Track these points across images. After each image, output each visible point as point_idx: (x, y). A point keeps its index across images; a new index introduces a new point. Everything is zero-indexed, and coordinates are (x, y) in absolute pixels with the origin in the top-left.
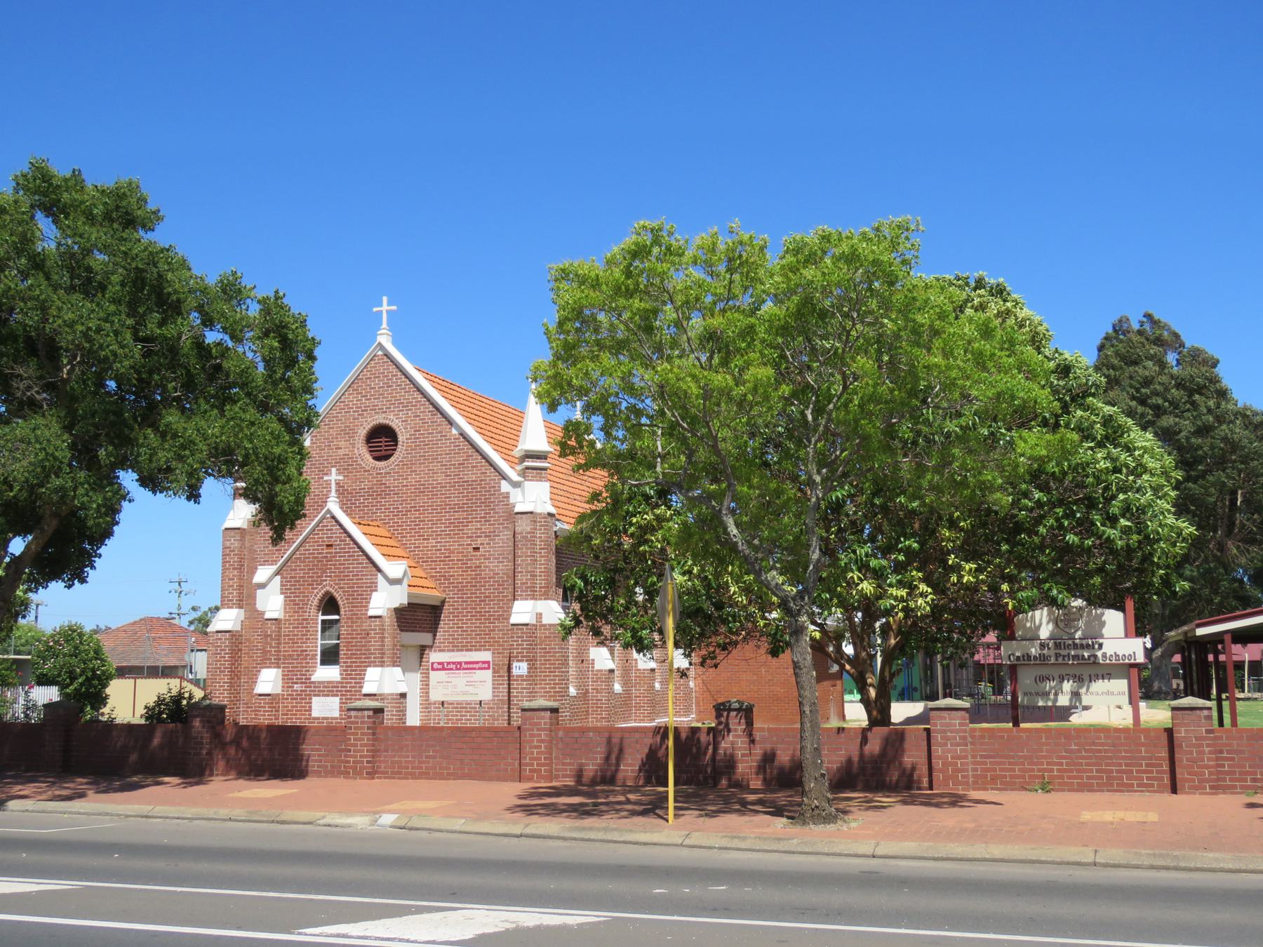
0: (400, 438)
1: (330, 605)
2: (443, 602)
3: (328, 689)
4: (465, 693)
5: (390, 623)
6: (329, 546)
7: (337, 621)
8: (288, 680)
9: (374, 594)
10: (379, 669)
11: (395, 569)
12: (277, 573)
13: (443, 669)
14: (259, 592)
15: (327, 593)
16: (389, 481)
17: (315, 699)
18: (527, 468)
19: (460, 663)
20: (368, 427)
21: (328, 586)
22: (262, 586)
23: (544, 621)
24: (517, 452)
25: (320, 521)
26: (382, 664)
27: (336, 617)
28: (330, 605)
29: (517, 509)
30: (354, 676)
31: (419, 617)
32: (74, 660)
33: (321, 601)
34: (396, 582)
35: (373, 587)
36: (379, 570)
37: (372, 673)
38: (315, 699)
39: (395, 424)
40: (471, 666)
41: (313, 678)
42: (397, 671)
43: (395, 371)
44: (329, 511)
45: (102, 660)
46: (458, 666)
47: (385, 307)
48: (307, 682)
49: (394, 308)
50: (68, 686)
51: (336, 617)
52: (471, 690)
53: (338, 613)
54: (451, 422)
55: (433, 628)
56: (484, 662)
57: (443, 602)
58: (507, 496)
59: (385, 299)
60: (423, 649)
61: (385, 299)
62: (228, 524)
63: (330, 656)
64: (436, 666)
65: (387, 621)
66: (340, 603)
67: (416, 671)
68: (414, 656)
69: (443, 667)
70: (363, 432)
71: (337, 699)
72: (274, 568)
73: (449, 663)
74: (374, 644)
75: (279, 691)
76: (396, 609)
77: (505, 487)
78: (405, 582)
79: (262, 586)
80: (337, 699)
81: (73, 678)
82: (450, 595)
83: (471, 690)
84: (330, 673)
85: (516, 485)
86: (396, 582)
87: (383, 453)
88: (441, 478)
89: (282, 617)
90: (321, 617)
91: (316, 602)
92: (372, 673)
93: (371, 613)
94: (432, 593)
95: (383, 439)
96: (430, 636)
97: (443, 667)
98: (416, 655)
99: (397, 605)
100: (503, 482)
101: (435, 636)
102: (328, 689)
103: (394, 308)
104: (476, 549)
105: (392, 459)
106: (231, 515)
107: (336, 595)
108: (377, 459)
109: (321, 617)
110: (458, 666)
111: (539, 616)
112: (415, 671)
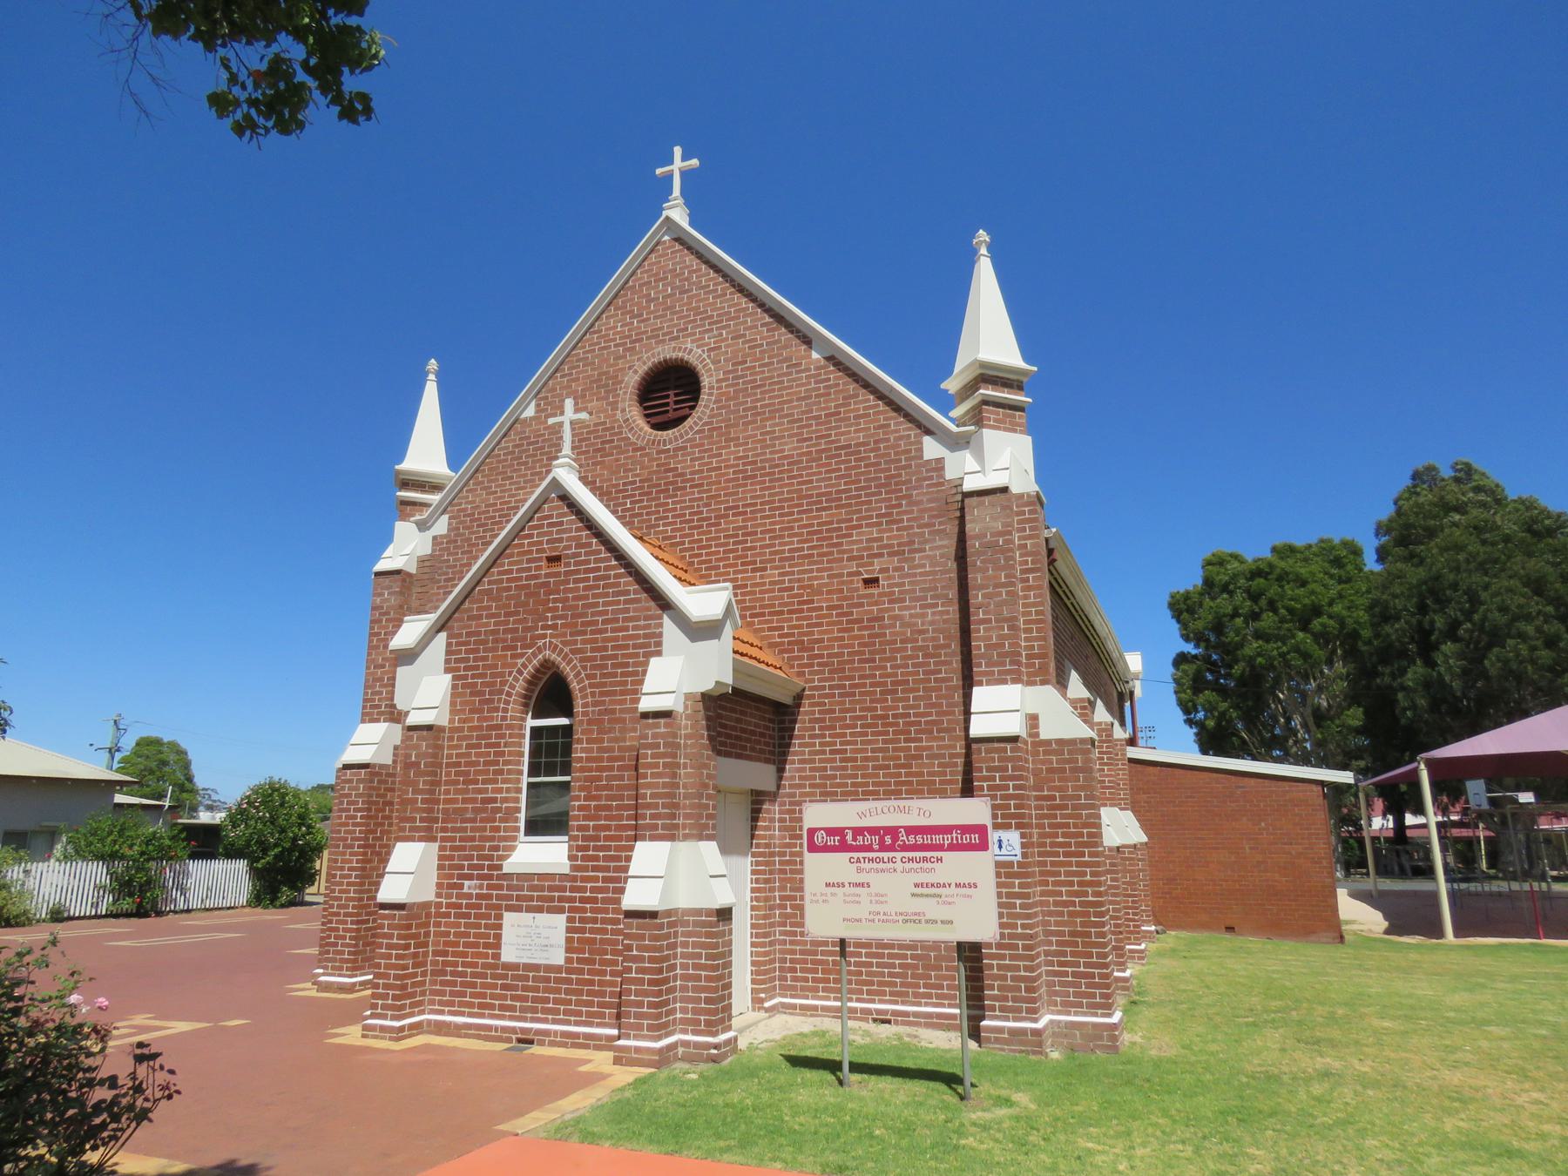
0: (706, 381)
1: (551, 693)
2: (799, 697)
3: (539, 893)
5: (691, 731)
6: (551, 560)
7: (568, 730)
8: (450, 872)
9: (654, 661)
10: (665, 846)
11: (705, 601)
12: (440, 627)
13: (843, 847)
14: (402, 672)
15: (546, 665)
16: (683, 464)
17: (508, 918)
18: (985, 402)
19: (893, 831)
21: (550, 648)
22: (408, 656)
23: (1046, 733)
24: (952, 385)
26: (670, 834)
27: (564, 721)
28: (551, 693)
31: (748, 722)
33: (531, 683)
36: (664, 603)
37: (648, 856)
38: (508, 918)
39: (693, 352)
45: (309, 827)
46: (888, 839)
47: (678, 164)
48: (491, 872)
49: (695, 162)
50: (257, 860)
51: (564, 721)
52: (930, 908)
53: (568, 712)
54: (807, 340)
55: (778, 755)
56: (966, 829)
57: (799, 697)
58: (939, 465)
59: (678, 151)
60: (757, 801)
61: (678, 151)
64: (820, 838)
65: (685, 726)
68: (738, 813)
69: (840, 841)
71: (560, 921)
72: (432, 617)
73: (858, 831)
74: (652, 783)
75: (428, 894)
76: (706, 697)
78: (728, 631)
80: (560, 921)
81: (265, 851)
82: (813, 681)
83: (930, 908)
84: (543, 855)
85: (957, 443)
87: (672, 415)
88: (789, 447)
89: (444, 721)
90: (531, 723)
91: (520, 686)
92: (648, 856)
93: (646, 704)
94: (777, 677)
95: (671, 393)
97: (840, 841)
98: (742, 812)
99: (707, 685)
100: (927, 440)
101: (781, 770)
102: (539, 893)
104: (871, 582)
105: (689, 421)
106: (388, 552)
107: (566, 669)
109: (531, 723)
110: (888, 839)
111: (1033, 720)
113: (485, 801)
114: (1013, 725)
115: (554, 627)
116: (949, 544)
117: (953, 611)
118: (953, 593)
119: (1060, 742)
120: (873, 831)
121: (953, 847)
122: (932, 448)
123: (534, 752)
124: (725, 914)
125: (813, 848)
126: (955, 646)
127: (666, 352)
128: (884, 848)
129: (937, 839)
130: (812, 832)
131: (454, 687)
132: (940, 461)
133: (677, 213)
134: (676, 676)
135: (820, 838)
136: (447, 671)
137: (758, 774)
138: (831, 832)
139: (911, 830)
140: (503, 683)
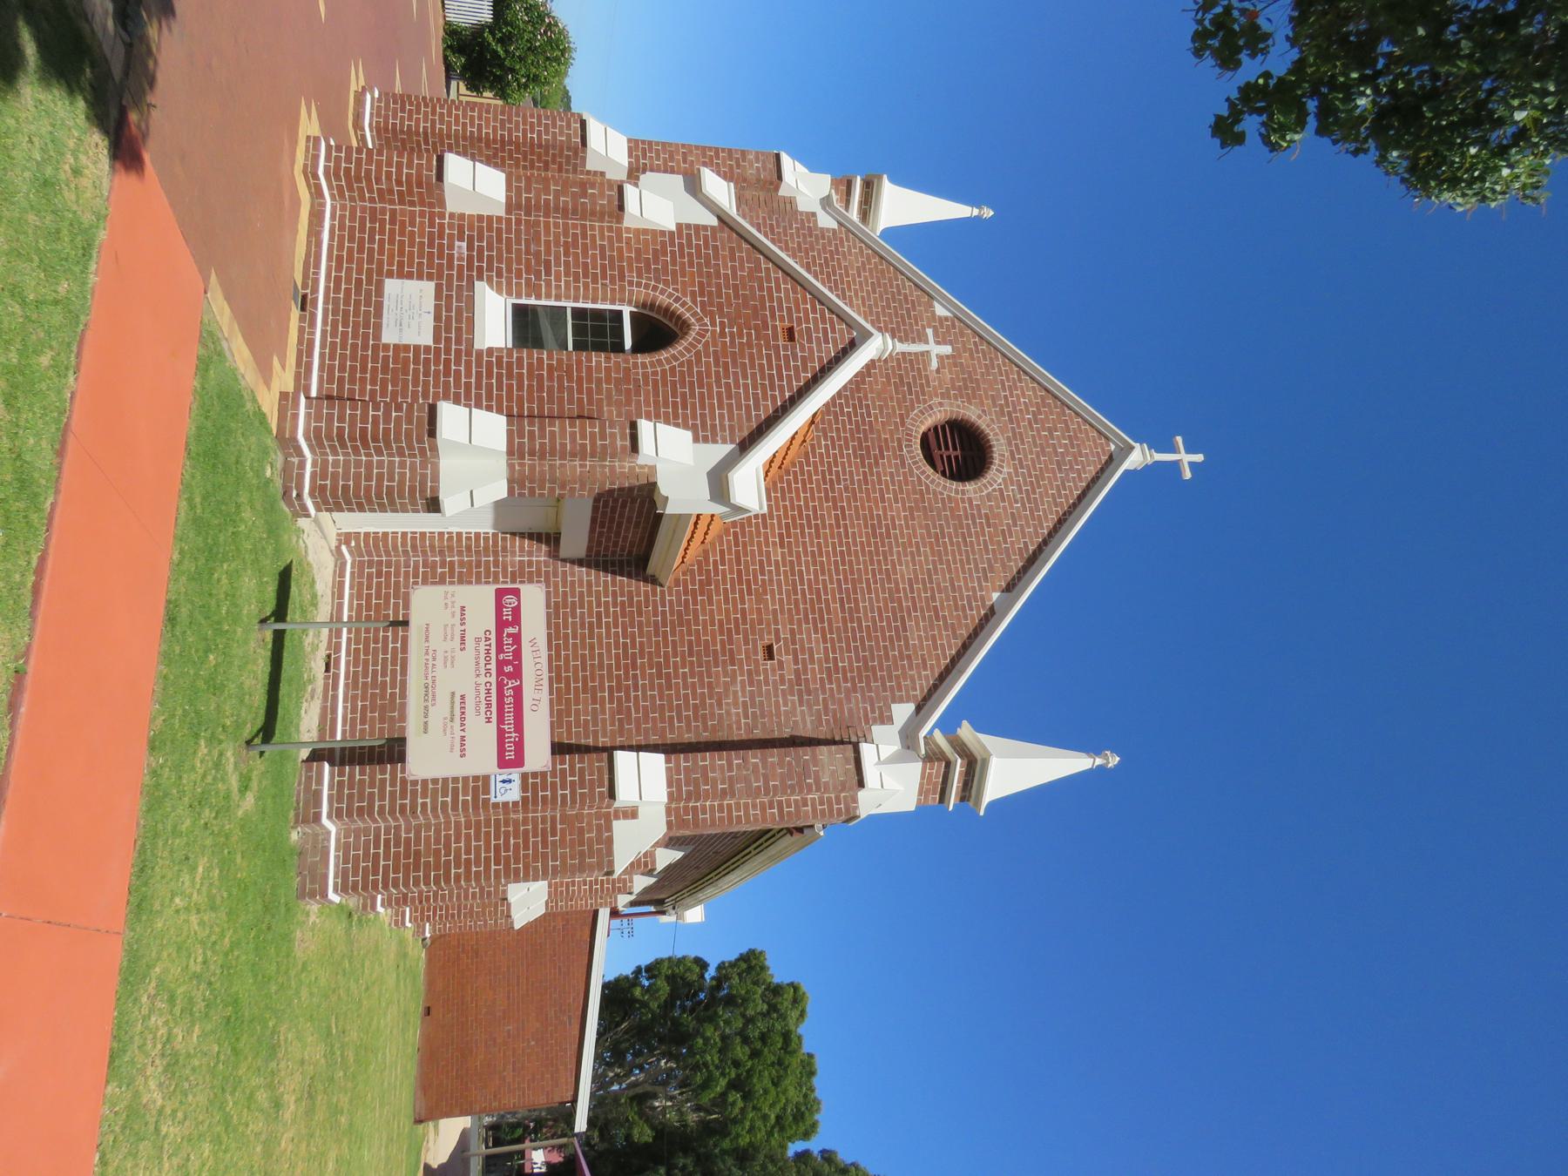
0: (970, 487)
1: (656, 332)
2: (654, 581)
3: (454, 317)
4: (429, 691)
5: (618, 472)
7: (618, 347)
8: (477, 228)
9: (689, 434)
10: (502, 446)
12: (724, 220)
13: (501, 624)
14: (678, 180)
15: (685, 326)
16: (887, 466)
17: (429, 287)
18: (948, 764)
19: (517, 674)
20: (982, 424)
21: (701, 330)
23: (618, 825)
24: (966, 731)
25: (842, 317)
27: (628, 344)
28: (656, 332)
29: (865, 748)
30: (483, 383)
31: (628, 530)
32: (523, 44)
33: (666, 311)
34: (718, 483)
35: (702, 435)
36: (746, 445)
37: (492, 428)
38: (429, 287)
39: (998, 474)
40: (508, 708)
41: (481, 287)
42: (499, 490)
43: (1088, 476)
44: (867, 336)
46: (509, 668)
48: (476, 269)
49: (1188, 475)
50: (492, 33)
51: (628, 344)
52: (440, 711)
53: (637, 348)
54: (1011, 587)
55: (599, 559)
56: (519, 746)
57: (654, 581)
59: (1199, 458)
60: (550, 539)
61: (1199, 458)
62: (786, 160)
63: (526, 323)
64: (510, 600)
65: (623, 466)
66: (664, 355)
67: (495, 526)
69: (507, 620)
70: (971, 413)
71: (427, 339)
73: (517, 639)
74: (565, 433)
75: (452, 206)
76: (652, 487)
77: (902, 712)
78: (718, 509)
79: (694, 186)
80: (427, 339)
81: (505, 40)
82: (669, 595)
83: (440, 711)
84: (493, 324)
85: (908, 737)
86: (718, 483)
87: (936, 453)
88: (904, 570)
89: (627, 223)
90: (627, 311)
91: (663, 300)
92: (492, 428)
93: (645, 427)
94: (674, 558)
96: (580, 550)
97: (507, 620)
98: (538, 523)
99: (664, 488)
100: (910, 708)
101: (580, 563)
103: (1188, 475)
105: (930, 471)
106: (801, 168)
107: (680, 347)
108: (925, 439)
109: (627, 311)
110: (509, 668)
111: (632, 813)
112: (497, 523)
113: (548, 263)
114: (626, 793)
115: (723, 334)
116: (807, 730)
117: (741, 734)
118: (758, 734)
119: (610, 841)
120: (518, 654)
121: (501, 734)
122: (902, 712)
123: (598, 315)
124: (434, 505)
125: (500, 594)
126: (705, 736)
127: (999, 447)
128: (501, 664)
129: (509, 718)
130: (516, 592)
131: (663, 233)
132: (890, 720)
133: (1138, 458)
134: (673, 457)
135: (510, 600)
136: (679, 226)
137: (576, 540)
138: (517, 612)
139: (518, 691)
140: (666, 283)
